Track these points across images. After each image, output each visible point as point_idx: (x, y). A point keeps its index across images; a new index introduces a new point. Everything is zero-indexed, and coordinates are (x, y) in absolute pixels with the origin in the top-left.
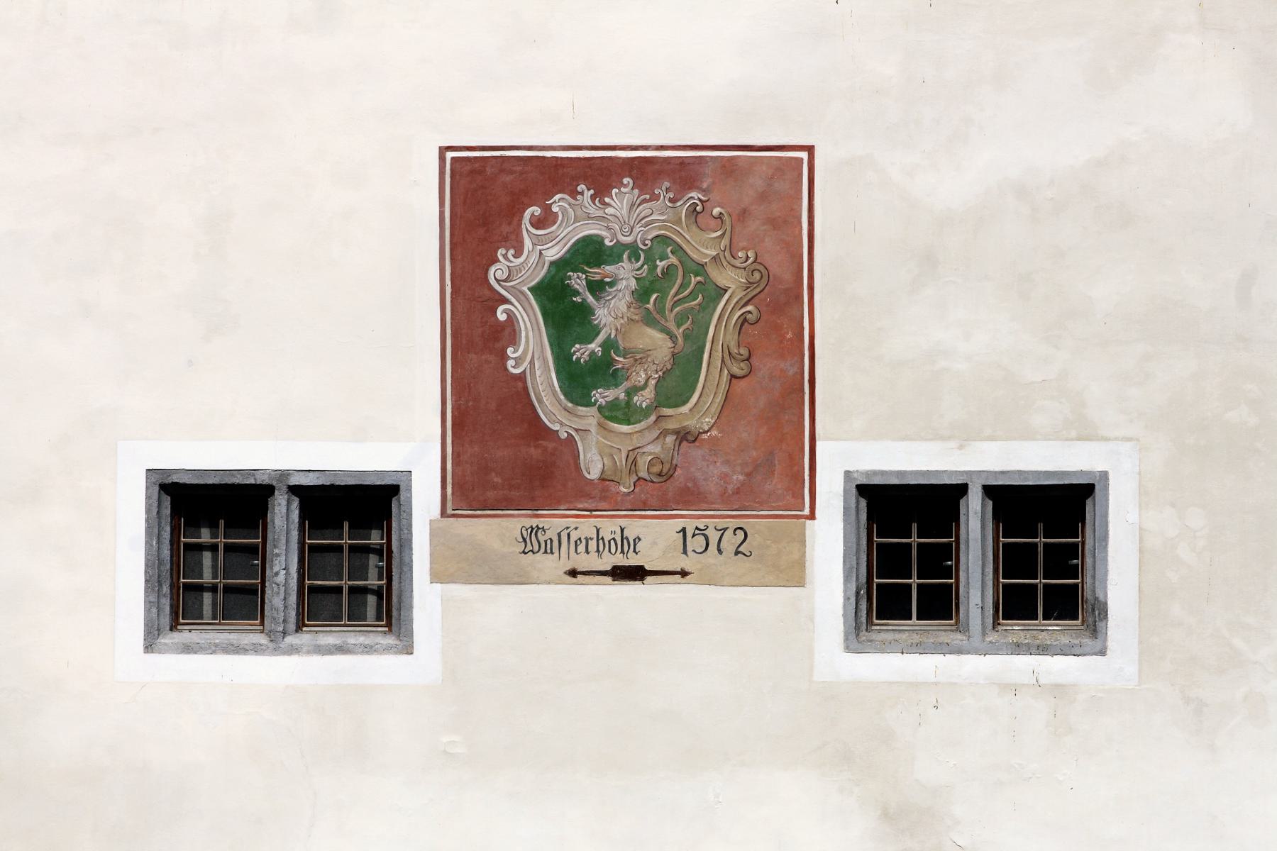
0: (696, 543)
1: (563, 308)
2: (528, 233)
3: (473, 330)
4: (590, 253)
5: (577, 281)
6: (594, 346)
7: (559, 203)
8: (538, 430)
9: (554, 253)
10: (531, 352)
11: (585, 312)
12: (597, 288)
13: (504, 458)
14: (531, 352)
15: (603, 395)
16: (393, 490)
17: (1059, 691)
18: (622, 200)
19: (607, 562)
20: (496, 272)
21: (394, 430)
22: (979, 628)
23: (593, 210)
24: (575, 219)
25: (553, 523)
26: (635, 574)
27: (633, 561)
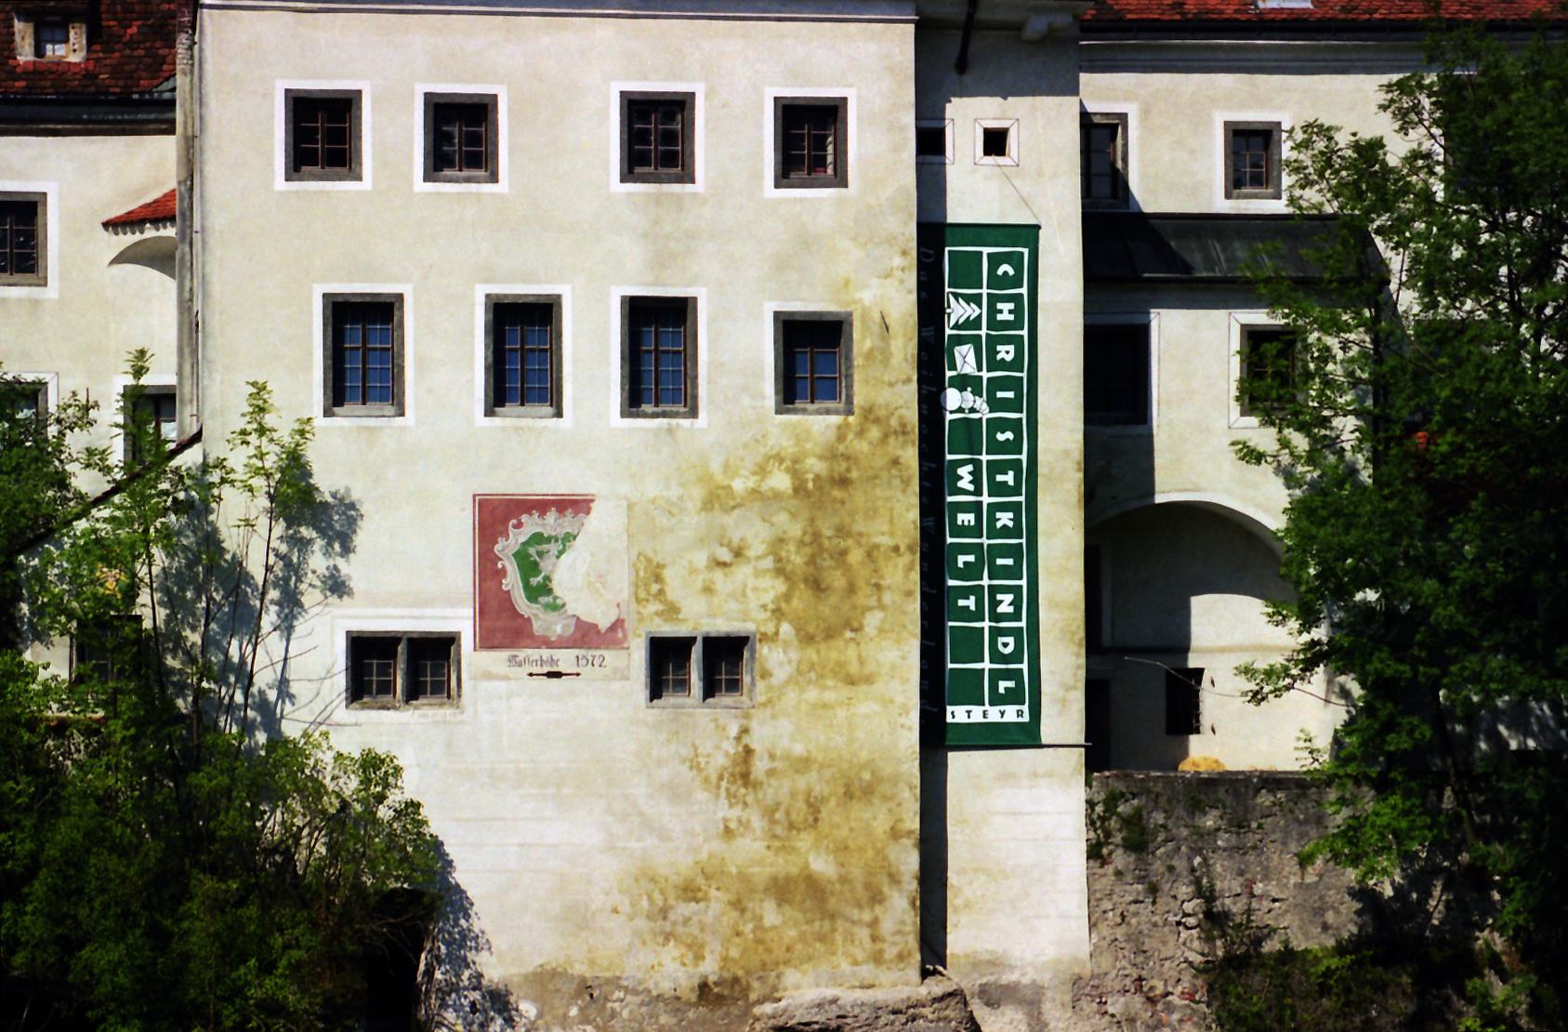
0: (583, 662)
1: (528, 566)
2: (511, 531)
3: (487, 568)
4: (538, 538)
5: (532, 551)
6: (540, 578)
7: (524, 518)
8: (515, 614)
9: (523, 539)
10: (512, 581)
11: (536, 564)
12: (540, 554)
13: (503, 627)
14: (512, 581)
15: (544, 600)
16: (391, 305)
17: (478, 195)
18: (551, 516)
19: (546, 669)
20: (497, 548)
21: (460, 620)
22: (870, 992)
23: (539, 521)
24: (531, 524)
25: (522, 654)
26: (558, 675)
27: (555, 669)
